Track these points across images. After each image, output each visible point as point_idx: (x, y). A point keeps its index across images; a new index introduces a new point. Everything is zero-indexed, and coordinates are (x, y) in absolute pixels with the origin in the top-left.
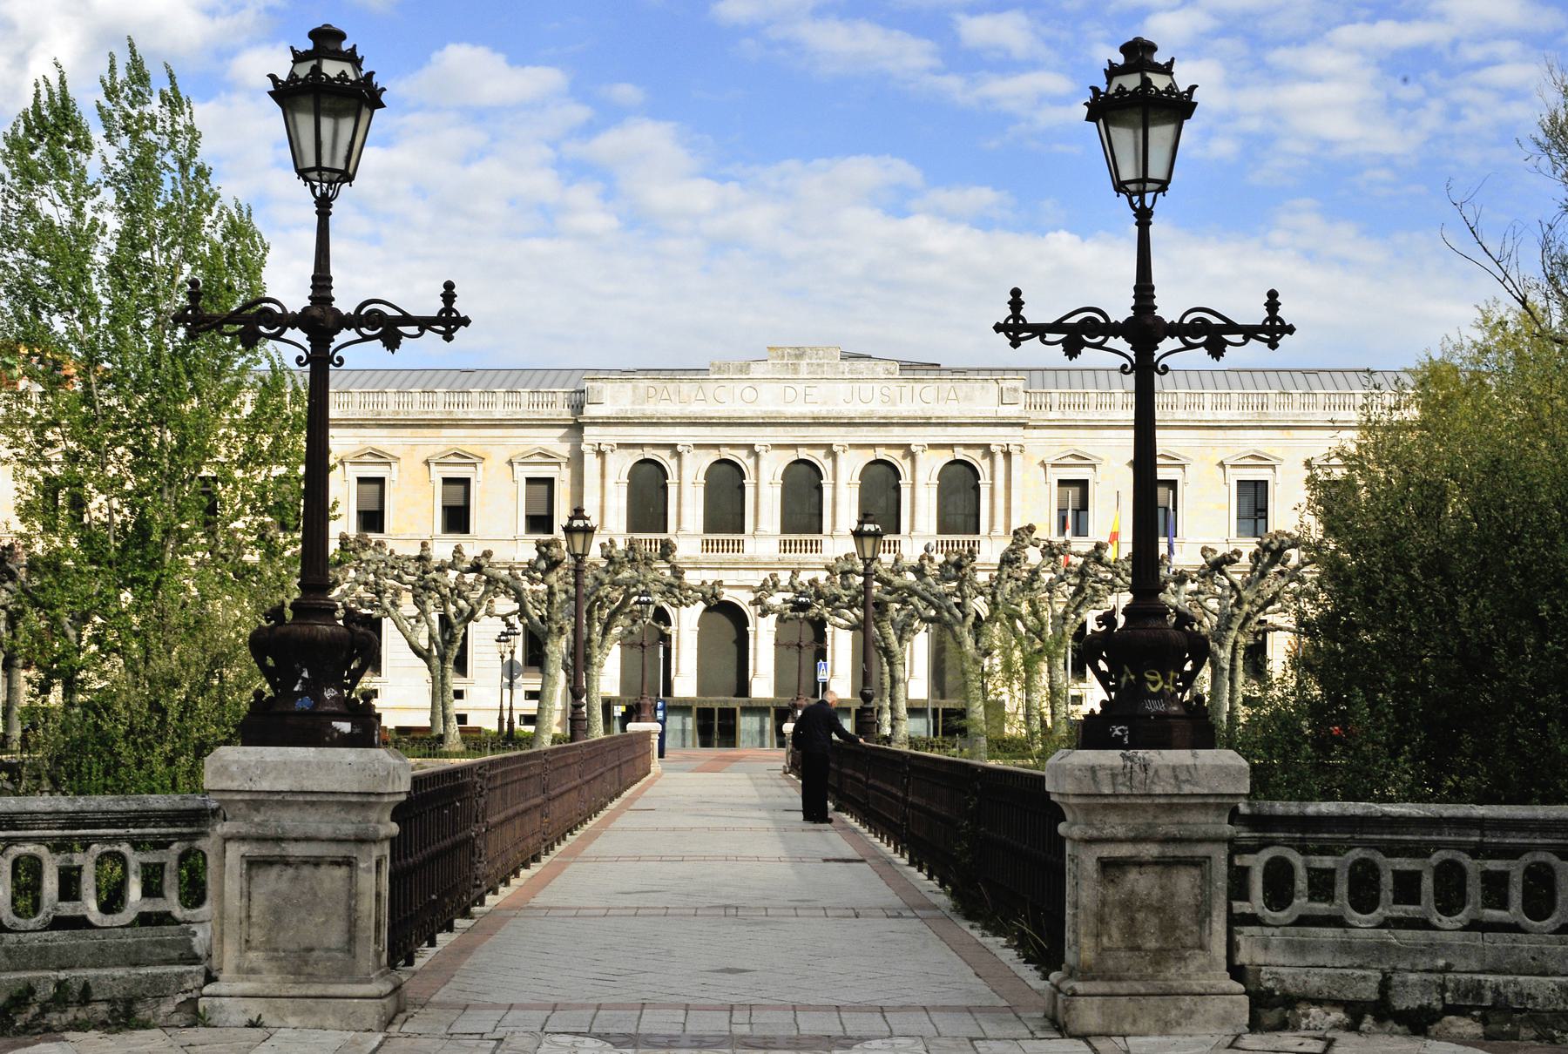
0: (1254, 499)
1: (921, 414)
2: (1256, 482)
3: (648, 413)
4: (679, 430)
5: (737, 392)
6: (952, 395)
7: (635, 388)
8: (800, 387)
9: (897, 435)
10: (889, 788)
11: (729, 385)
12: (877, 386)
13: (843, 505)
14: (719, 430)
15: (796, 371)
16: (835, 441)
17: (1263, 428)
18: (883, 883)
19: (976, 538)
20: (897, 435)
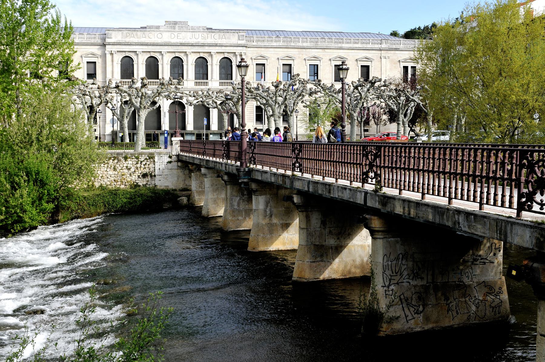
3: (127, 41)
4: (137, 47)
5: (156, 35)
6: (224, 37)
7: (122, 33)
8: (176, 34)
9: (207, 49)
11: (153, 33)
12: (200, 34)
14: (150, 47)
15: (174, 29)
17: (317, 49)
20: (207, 49)
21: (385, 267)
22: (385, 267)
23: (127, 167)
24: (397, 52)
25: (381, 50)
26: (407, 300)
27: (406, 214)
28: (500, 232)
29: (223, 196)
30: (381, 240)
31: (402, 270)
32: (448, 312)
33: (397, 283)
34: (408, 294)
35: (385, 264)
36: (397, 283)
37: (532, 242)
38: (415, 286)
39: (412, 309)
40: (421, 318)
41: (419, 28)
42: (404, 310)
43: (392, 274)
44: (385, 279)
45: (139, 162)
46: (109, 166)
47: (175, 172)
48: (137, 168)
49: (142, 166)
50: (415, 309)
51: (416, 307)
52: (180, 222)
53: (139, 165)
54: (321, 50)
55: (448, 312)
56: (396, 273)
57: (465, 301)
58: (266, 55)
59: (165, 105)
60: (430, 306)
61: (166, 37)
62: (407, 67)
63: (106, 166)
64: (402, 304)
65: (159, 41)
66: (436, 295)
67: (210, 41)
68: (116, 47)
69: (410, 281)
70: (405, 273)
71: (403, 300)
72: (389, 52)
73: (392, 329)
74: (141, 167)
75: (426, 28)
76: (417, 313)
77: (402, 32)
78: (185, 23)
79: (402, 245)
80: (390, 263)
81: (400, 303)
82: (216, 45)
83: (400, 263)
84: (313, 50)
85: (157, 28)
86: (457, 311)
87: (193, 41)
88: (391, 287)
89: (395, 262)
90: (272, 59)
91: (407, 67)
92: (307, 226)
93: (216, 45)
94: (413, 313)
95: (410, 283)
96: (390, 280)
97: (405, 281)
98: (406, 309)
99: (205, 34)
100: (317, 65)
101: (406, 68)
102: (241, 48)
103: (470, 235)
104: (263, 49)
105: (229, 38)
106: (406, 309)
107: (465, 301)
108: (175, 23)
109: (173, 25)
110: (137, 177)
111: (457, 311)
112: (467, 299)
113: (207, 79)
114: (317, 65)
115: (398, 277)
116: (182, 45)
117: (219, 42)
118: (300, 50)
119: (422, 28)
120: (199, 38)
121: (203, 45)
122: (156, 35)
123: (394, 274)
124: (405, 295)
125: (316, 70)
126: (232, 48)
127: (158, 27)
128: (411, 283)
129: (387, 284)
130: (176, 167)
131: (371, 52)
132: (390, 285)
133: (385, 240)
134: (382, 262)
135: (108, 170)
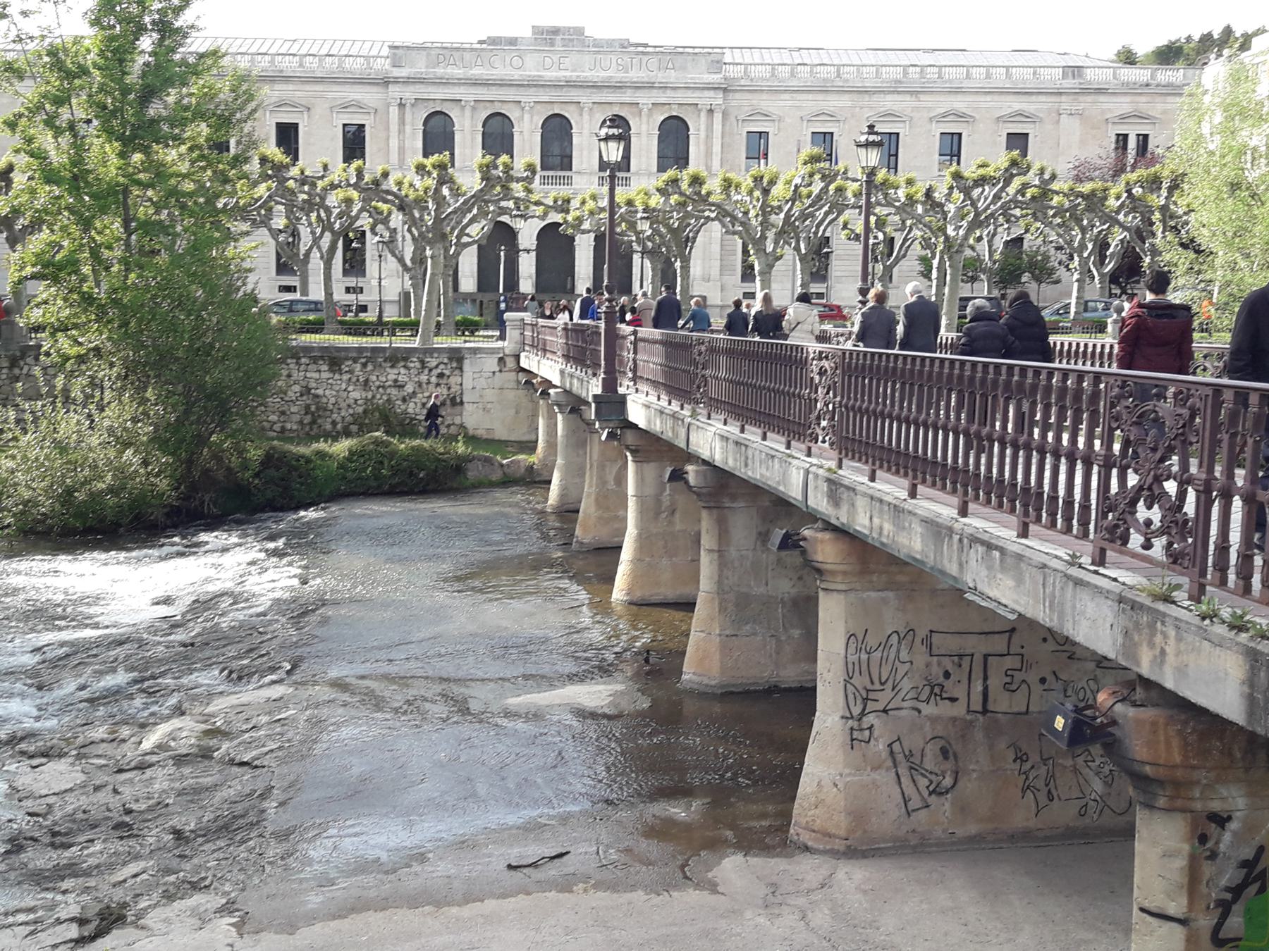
0: (952, 147)
1: (646, 80)
2: (825, 133)
3: (439, 75)
4: (462, 90)
5: (508, 60)
6: (670, 65)
7: (428, 55)
8: (555, 58)
9: (627, 97)
10: (799, 272)
11: (502, 54)
12: (614, 58)
13: (588, 147)
14: (494, 90)
15: (552, 45)
16: (583, 100)
17: (899, 92)
18: (1113, 146)
19: (627, 175)
20: (627, 97)
21: (850, 666)
22: (850, 666)
23: (396, 381)
24: (1102, 98)
25: (1061, 93)
26: (909, 756)
27: (875, 535)
28: (1051, 603)
29: (163, 484)
30: (842, 596)
31: (899, 677)
32: (1024, 792)
33: (885, 711)
34: (914, 742)
35: (851, 658)
36: (885, 711)
37: (1115, 641)
38: (934, 720)
39: (923, 782)
40: (947, 806)
41: (1189, 39)
42: (900, 783)
43: (870, 687)
44: (851, 697)
45: (426, 371)
46: (354, 379)
47: (511, 395)
48: (420, 384)
49: (434, 379)
50: (931, 782)
51: (933, 777)
52: (395, 529)
53: (424, 378)
54: (908, 97)
55: (1024, 792)
56: (882, 684)
57: (1074, 766)
58: (771, 109)
59: (528, 233)
60: (975, 775)
61: (532, 67)
62: (1126, 136)
63: (346, 377)
64: (895, 766)
65: (516, 75)
66: (991, 747)
67: (636, 75)
68: (411, 88)
69: (922, 706)
70: (906, 685)
71: (900, 757)
72: (1081, 98)
73: (865, 831)
74: (429, 383)
75: (1207, 39)
76: (937, 792)
77: (1143, 48)
78: (579, 31)
79: (898, 609)
80: (864, 657)
81: (889, 763)
82: (650, 86)
83: (892, 656)
84: (889, 97)
85: (511, 44)
86: (1049, 792)
87: (597, 75)
88: (865, 719)
89: (878, 654)
90: (788, 120)
91: (1126, 136)
92: (720, 545)
93: (650, 86)
94: (925, 794)
95: (920, 712)
96: (865, 700)
97: (905, 704)
98: (906, 781)
99: (626, 58)
100: (898, 134)
101: (1122, 139)
102: (711, 94)
103: (992, 605)
104: (765, 96)
105: (684, 68)
106: (906, 781)
107: (1074, 766)
108: (556, 31)
109: (548, 36)
110: (419, 405)
111: (1049, 792)
112: (1080, 760)
113: (629, 170)
114: (898, 134)
115: (888, 693)
116: (571, 84)
117: (660, 77)
118: (855, 96)
119: (1196, 37)
120: (609, 70)
121: (619, 87)
122: (508, 60)
123: (878, 686)
124: (905, 744)
125: (955, 148)
126: (689, 93)
127: (513, 41)
128: (924, 712)
129: (856, 711)
130: (513, 385)
131: (1034, 98)
132: (863, 714)
133: (852, 595)
134: (843, 652)
135: (351, 388)
